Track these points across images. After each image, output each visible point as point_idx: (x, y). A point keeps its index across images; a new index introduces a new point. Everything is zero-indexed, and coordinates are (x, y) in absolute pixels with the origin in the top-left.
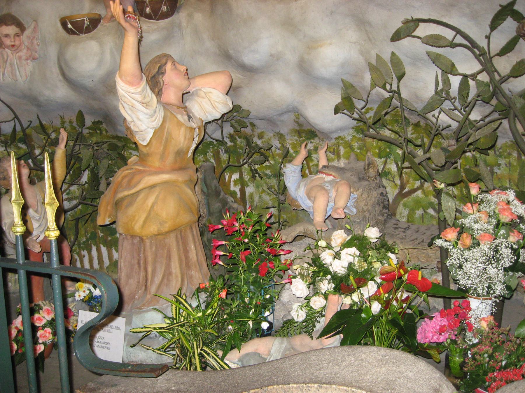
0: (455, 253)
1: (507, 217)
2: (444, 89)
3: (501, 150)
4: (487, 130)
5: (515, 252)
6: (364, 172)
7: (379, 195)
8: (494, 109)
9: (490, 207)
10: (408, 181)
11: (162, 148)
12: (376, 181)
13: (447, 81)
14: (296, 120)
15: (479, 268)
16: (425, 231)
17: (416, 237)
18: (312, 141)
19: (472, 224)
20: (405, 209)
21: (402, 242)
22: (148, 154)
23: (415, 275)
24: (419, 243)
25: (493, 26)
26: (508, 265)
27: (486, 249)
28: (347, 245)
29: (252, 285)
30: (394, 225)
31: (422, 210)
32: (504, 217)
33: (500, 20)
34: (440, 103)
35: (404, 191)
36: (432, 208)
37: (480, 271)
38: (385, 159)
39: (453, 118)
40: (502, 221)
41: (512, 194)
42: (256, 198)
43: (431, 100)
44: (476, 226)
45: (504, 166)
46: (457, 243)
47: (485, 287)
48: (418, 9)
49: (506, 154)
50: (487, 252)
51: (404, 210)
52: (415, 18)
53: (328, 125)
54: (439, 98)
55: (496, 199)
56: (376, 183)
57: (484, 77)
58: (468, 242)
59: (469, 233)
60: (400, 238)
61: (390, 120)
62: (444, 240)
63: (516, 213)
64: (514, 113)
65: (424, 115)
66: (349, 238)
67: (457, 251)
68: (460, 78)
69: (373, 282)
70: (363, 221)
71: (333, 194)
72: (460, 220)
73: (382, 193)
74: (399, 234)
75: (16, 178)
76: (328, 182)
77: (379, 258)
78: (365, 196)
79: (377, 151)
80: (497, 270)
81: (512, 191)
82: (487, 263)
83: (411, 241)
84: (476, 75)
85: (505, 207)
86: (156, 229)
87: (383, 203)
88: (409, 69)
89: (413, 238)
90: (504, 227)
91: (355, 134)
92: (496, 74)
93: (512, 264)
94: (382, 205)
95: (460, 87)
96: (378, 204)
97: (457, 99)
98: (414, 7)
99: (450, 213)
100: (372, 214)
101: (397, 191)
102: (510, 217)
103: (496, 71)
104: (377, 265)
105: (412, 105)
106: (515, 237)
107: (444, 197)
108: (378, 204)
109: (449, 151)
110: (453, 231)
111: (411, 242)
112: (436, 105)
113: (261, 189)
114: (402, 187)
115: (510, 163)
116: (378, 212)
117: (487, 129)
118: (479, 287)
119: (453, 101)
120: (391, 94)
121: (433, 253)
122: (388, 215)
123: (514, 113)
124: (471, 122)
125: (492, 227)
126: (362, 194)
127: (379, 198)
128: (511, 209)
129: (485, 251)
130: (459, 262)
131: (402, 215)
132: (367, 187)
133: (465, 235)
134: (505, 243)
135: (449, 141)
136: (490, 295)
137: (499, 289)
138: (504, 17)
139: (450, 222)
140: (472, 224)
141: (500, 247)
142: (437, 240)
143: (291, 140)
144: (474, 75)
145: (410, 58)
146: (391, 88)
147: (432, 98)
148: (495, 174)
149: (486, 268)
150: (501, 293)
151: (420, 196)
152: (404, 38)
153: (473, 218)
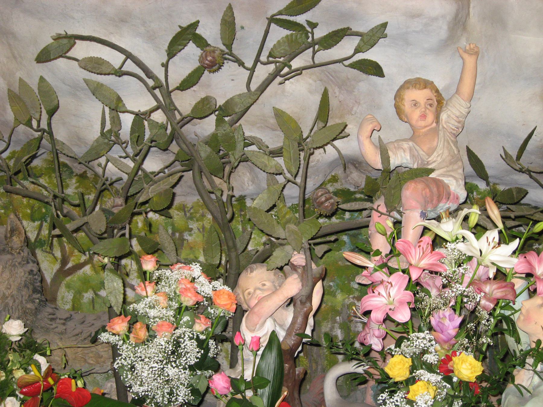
0: (125, 350)
1: (189, 299)
2: (113, 129)
3: (192, 211)
4: (164, 186)
5: (202, 344)
6: (5, 242)
7: (27, 274)
8: (176, 157)
10: (72, 253)
12: (22, 255)
13: (116, 119)
15: (154, 369)
16: (93, 322)
17: (81, 331)
19: (148, 310)
20: (68, 292)
21: (61, 339)
23: (67, 385)
24: (85, 339)
25: (172, 52)
26: (194, 362)
27: (163, 343)
30: (50, 314)
31: (92, 292)
32: (187, 299)
33: (180, 45)
34: (107, 149)
37: (155, 374)
38: (39, 222)
39: (121, 169)
40: (184, 304)
41: (198, 269)
43: (95, 144)
44: (152, 313)
45: (196, 231)
46: (128, 337)
47: (166, 394)
48: (79, 22)
49: (198, 215)
50: (164, 347)
51: (67, 294)
52: (70, 33)
54: (106, 141)
55: (177, 276)
56: (23, 257)
57: (159, 117)
58: (143, 334)
59: (143, 322)
60: (59, 333)
62: (111, 333)
63: (202, 293)
64: (199, 166)
65: (87, 164)
67: (127, 348)
68: (132, 117)
69: (15, 399)
70: (4, 311)
72: (132, 306)
73: (32, 271)
74: (57, 327)
75: (306, 157)
77: (22, 363)
79: (29, 211)
80: (177, 371)
81: (198, 265)
82: (165, 361)
83: (74, 336)
84: (148, 113)
85: (189, 286)
87: (33, 285)
88: (63, 101)
89: (77, 332)
90: (187, 312)
92: (176, 112)
93: (198, 360)
94: (31, 287)
95: (132, 128)
96: (26, 286)
97: (130, 143)
98: (74, 18)
99: (116, 297)
100: (17, 301)
101: (57, 266)
102: (194, 298)
103: (176, 109)
104: (19, 374)
105: (69, 149)
106: (202, 325)
107: (107, 275)
108: (26, 286)
109: (113, 213)
110: (123, 321)
111: (74, 338)
112: (102, 150)
114: (64, 261)
115: (204, 228)
117: (163, 183)
118: (158, 394)
119: (124, 145)
120: (40, 133)
121: (105, 351)
122: (41, 301)
123: (199, 166)
124: (146, 174)
125: (172, 313)
127: (27, 278)
128: (195, 289)
129: (162, 345)
130: (130, 363)
131: (65, 300)
132: (9, 263)
133: (138, 325)
134: (188, 333)
135: (114, 200)
136: (172, 404)
137: (182, 395)
138: (185, 42)
139: (117, 309)
140: (148, 310)
141: (183, 338)
142: (103, 334)
144: (147, 113)
145: (68, 85)
146: (39, 125)
147: (97, 141)
148: (185, 242)
149: (164, 367)
150: (184, 400)
151: (89, 273)
152: (56, 59)
153: (147, 303)
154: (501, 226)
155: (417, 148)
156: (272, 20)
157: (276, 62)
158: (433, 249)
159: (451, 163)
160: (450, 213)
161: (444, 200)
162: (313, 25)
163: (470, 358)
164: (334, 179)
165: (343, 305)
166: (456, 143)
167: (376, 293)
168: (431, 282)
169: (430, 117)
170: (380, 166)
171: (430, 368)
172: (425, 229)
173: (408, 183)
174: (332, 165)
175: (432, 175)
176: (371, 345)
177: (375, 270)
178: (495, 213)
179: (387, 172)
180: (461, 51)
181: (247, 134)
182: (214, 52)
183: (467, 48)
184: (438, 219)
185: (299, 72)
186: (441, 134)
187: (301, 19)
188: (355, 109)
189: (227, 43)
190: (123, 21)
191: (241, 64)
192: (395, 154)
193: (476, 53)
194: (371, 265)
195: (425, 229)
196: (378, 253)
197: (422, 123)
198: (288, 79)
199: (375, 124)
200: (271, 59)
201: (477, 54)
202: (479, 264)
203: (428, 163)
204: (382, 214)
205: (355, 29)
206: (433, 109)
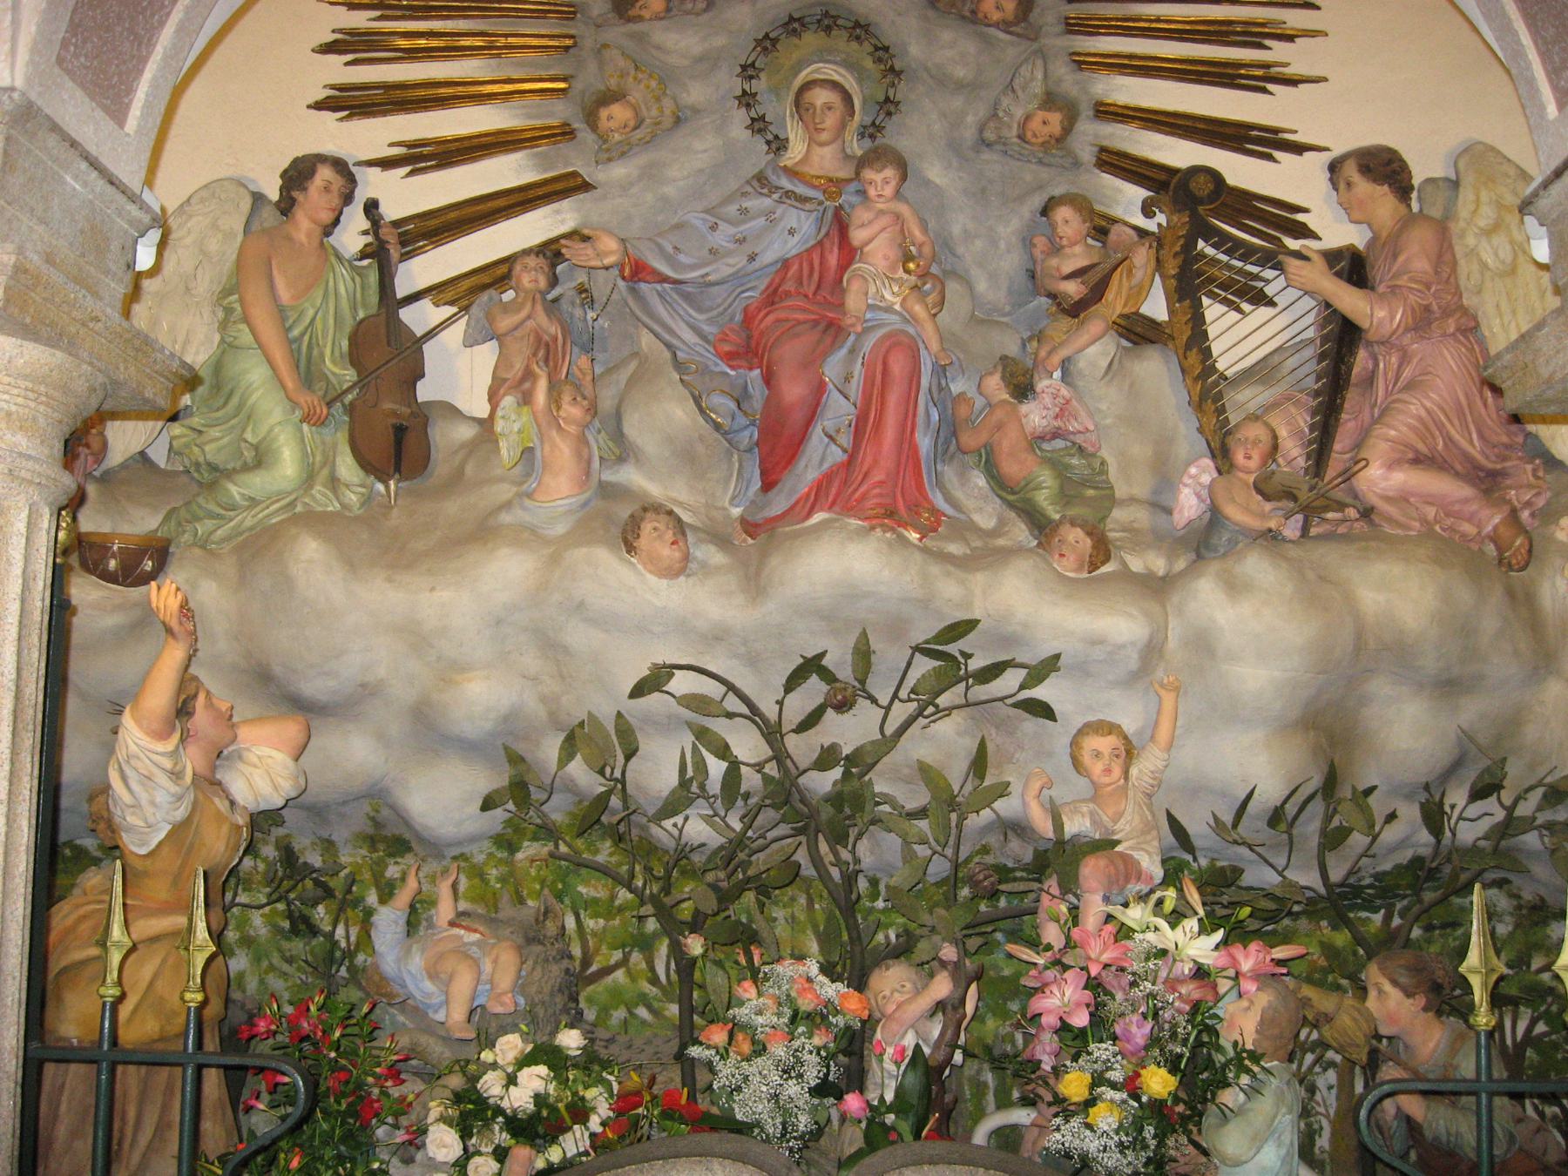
9: (779, 988)
10: (597, 951)
11: (179, 862)
14: (372, 814)
18: (399, 860)
22: (145, 872)
28: (525, 1061)
29: (343, 1143)
35: (589, 972)
36: (645, 1005)
40: (803, 1008)
42: (252, 985)
45: (783, 922)
53: (450, 828)
58: (746, 1048)
61: (567, 826)
66: (529, 1048)
71: (487, 966)
76: (473, 944)
78: (538, 974)
85: (807, 986)
86: (157, 1029)
91: (494, 849)
94: (566, 992)
96: (560, 990)
113: (265, 964)
114: (586, 962)
115: (793, 917)
116: (559, 1006)
119: (712, 800)
126: (533, 969)
143: (351, 855)
146: (612, 773)
147: (673, 792)
154: (1201, 912)
155: (1100, 812)
156: (917, 649)
157: (918, 700)
158: (1116, 941)
159: (1143, 833)
160: (1140, 897)
161: (1133, 881)
162: (967, 656)
163: (1163, 1072)
164: (985, 850)
165: (996, 1036)
166: (1150, 807)
167: (1048, 992)
168: (1116, 984)
169: (1117, 771)
170: (1051, 835)
171: (1114, 1086)
172: (1109, 918)
173: (1087, 859)
174: (987, 829)
175: (1119, 848)
176: (1040, 1061)
177: (1046, 968)
178: (1194, 897)
179: (1060, 843)
180: (1157, 686)
181: (877, 789)
182: (845, 689)
183: (1165, 681)
184: (1126, 905)
185: (949, 710)
186: (1131, 794)
187: (952, 649)
188: (1017, 756)
189: (859, 677)
190: (718, 639)
191: (874, 701)
192: (1071, 820)
193: (1177, 690)
194: (1041, 961)
195: (1109, 918)
196: (1049, 947)
197: (1107, 780)
198: (934, 721)
199: (1045, 780)
200: (913, 696)
201: (1177, 690)
202: (1175, 960)
203: (1113, 833)
204: (1054, 897)
205: (1019, 660)
206: (1120, 761)
